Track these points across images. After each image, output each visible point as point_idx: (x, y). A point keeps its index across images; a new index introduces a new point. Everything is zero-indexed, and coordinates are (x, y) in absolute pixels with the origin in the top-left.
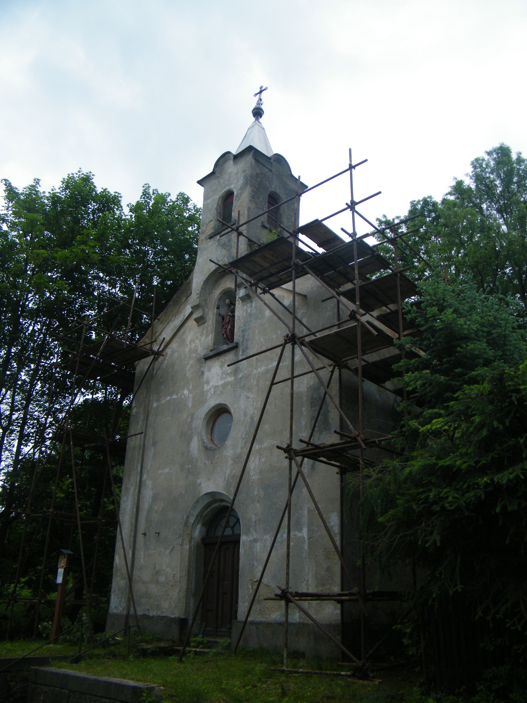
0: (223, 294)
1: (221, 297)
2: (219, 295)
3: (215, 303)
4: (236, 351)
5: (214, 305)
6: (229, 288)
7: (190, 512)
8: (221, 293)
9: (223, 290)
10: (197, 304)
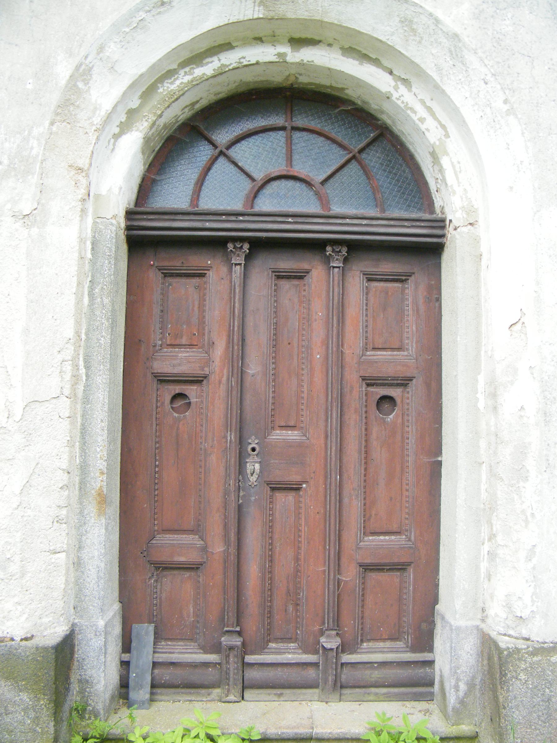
7: (101, 49)
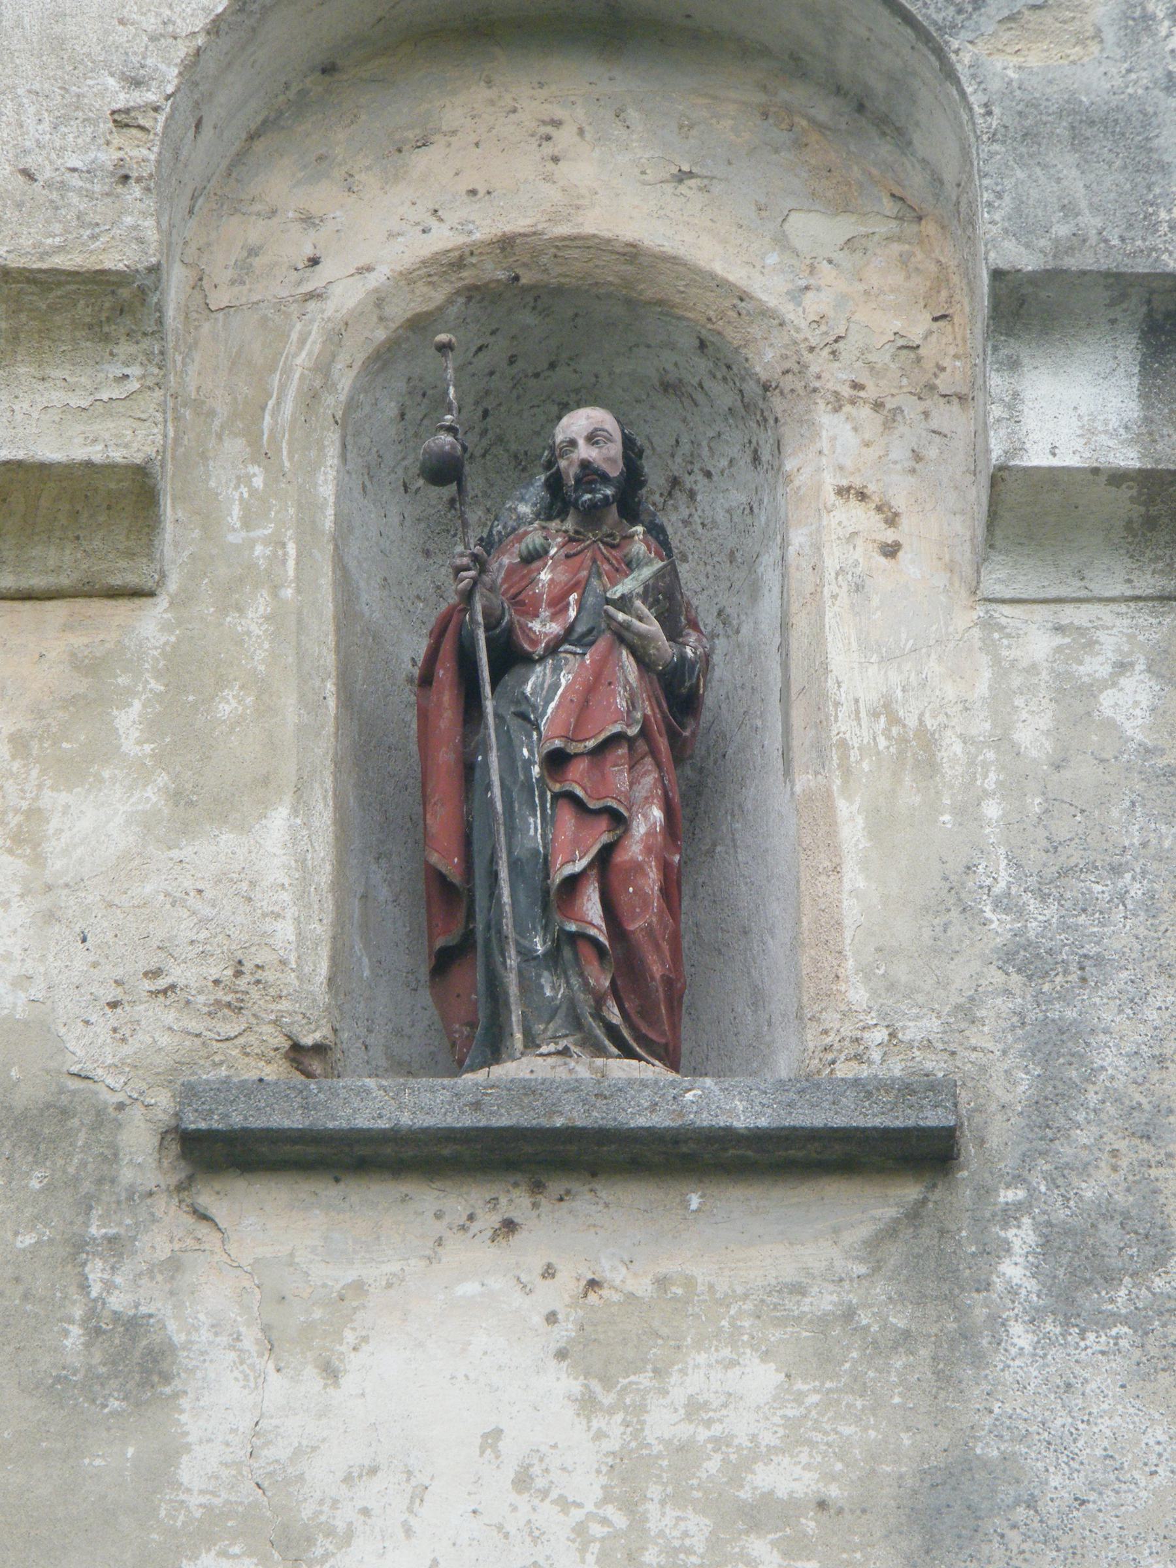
0: (473, 293)
1: (419, 325)
2: (408, 278)
3: (323, 368)
4: (914, 1215)
5: (311, 399)
6: (632, 254)
8: (457, 262)
9: (506, 243)
10: (113, 261)
